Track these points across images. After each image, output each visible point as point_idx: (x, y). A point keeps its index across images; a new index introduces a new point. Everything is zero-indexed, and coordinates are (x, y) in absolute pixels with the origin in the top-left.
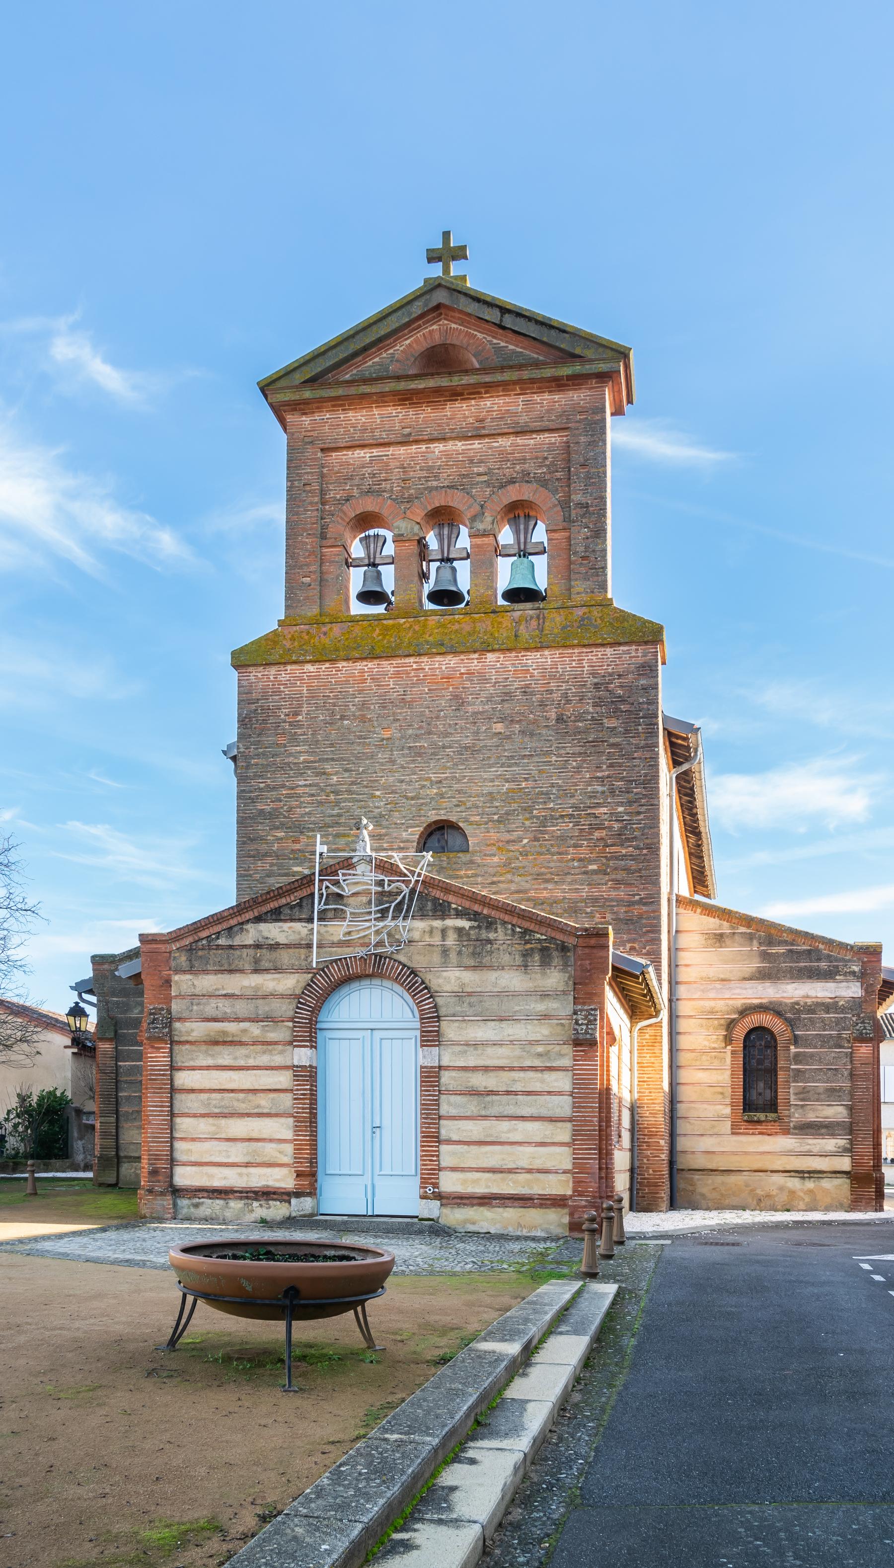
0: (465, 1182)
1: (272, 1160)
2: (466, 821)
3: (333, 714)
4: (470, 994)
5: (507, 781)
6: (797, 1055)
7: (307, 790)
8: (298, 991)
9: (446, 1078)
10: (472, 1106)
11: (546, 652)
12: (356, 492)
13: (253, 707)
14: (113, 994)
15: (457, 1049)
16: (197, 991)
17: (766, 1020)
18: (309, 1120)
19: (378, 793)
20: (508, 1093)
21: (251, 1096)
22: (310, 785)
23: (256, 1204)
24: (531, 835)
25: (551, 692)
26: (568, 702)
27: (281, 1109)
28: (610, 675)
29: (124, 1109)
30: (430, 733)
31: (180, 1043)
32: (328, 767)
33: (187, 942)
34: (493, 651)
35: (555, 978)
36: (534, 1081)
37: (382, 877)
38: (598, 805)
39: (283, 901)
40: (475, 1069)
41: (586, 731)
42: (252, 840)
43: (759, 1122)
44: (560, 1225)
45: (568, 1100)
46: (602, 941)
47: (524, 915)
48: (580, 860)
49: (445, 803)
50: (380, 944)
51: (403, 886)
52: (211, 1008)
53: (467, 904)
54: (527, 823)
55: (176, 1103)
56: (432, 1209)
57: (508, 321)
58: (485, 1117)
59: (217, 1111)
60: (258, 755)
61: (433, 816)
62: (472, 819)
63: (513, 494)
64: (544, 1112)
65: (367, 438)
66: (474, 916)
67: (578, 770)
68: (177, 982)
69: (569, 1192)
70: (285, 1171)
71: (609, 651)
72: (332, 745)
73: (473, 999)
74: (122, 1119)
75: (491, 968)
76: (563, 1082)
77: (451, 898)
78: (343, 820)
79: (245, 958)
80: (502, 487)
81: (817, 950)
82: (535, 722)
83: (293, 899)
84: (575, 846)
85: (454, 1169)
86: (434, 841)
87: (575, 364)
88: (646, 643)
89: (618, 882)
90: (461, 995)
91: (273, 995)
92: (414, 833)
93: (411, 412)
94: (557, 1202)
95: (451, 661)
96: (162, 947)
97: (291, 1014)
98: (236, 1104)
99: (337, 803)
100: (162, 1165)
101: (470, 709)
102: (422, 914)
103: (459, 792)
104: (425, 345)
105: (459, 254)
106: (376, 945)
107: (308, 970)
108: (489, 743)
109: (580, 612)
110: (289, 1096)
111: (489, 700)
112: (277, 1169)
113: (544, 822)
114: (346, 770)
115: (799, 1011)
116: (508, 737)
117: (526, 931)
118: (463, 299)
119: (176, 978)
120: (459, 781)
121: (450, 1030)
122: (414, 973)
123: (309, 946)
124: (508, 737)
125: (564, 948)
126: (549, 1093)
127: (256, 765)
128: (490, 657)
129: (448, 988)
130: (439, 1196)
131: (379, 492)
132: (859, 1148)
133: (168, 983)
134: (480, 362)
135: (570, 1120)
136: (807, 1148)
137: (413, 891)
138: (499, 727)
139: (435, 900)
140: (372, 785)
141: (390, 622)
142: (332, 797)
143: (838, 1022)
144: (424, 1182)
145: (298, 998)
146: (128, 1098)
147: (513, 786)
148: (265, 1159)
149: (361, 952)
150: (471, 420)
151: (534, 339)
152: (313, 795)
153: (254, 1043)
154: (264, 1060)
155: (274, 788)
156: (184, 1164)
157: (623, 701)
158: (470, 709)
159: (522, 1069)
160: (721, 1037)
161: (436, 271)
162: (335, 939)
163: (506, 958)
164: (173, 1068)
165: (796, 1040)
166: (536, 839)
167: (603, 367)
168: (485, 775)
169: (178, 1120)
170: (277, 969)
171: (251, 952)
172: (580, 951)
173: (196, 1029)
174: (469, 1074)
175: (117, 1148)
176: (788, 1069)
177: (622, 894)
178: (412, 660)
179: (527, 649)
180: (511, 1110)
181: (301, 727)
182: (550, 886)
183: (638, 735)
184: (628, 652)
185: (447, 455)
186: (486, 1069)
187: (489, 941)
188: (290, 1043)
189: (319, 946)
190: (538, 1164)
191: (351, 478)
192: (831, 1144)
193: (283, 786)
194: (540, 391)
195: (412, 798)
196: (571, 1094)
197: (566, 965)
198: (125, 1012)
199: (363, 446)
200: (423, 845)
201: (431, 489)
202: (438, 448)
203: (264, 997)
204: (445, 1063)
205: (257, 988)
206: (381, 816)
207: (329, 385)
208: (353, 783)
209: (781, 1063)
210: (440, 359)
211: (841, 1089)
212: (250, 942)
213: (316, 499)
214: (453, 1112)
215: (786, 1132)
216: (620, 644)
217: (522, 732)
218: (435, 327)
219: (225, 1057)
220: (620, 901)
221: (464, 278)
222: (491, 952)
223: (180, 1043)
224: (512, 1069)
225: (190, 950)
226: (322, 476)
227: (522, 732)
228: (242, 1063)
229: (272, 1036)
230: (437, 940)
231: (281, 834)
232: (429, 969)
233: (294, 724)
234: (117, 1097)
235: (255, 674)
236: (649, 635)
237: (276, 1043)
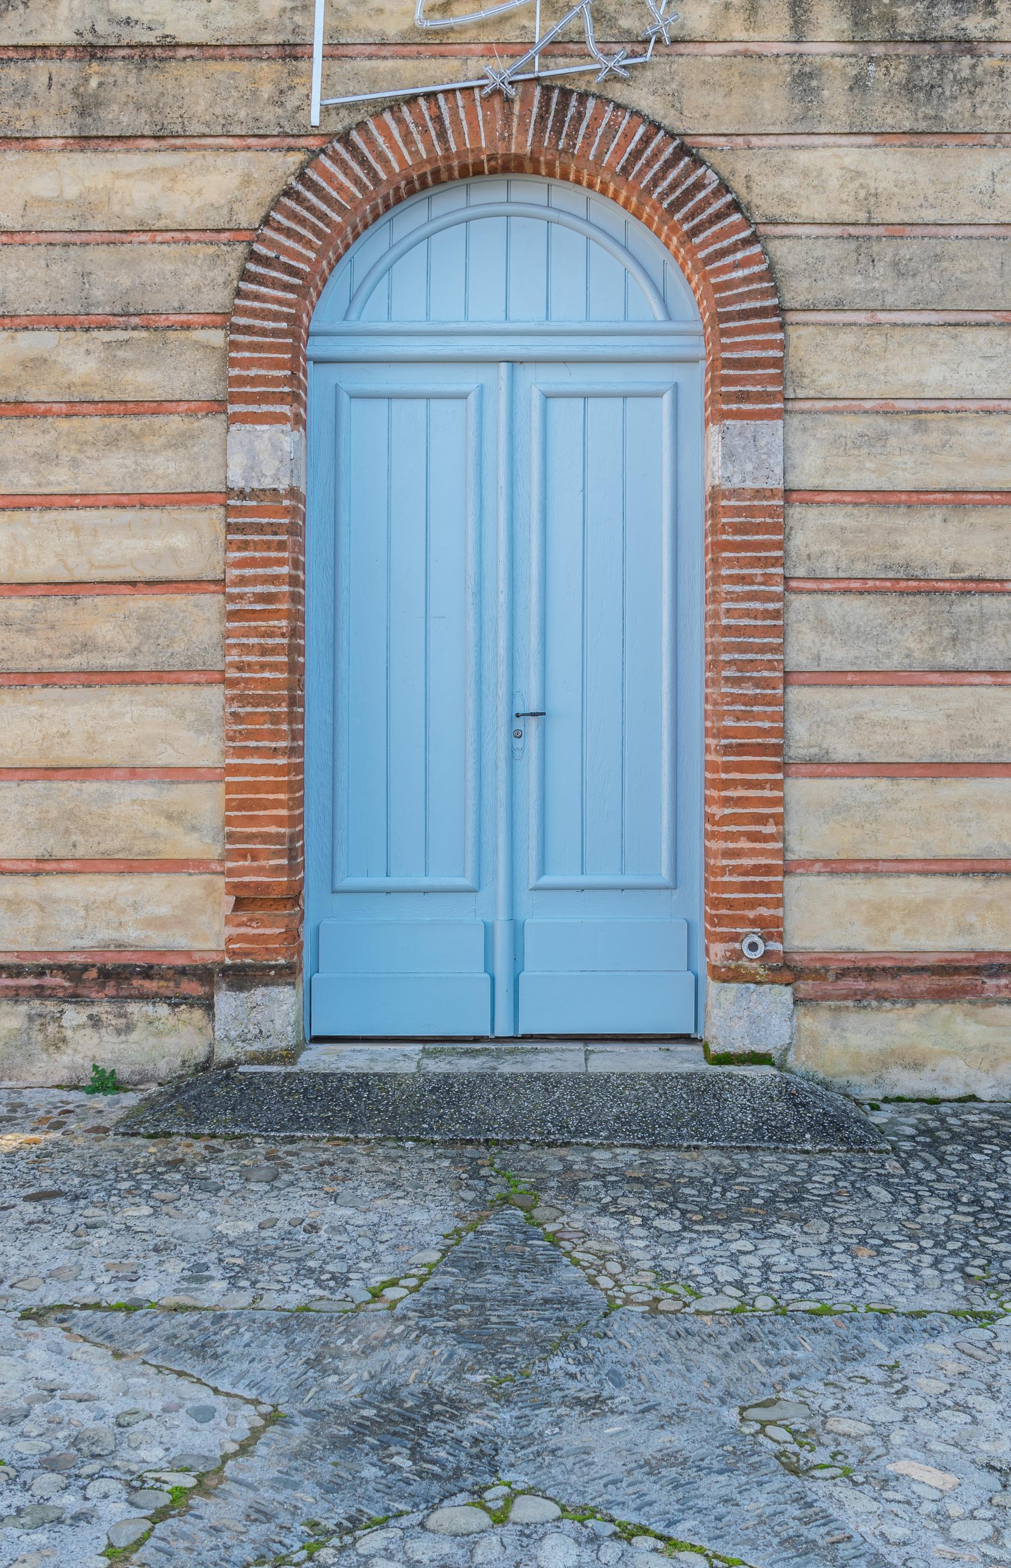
1: (139, 848)
4: (897, 231)
8: (248, 216)
9: (810, 533)
10: (907, 635)
15: (854, 425)
21: (57, 608)
23: (74, 1016)
40: (916, 499)
56: (750, 1018)
58: (956, 675)
70: (188, 887)
73: (908, 250)
75: (970, 137)
85: (838, 867)
90: (865, 233)
97: (219, 298)
110: (212, 603)
112: (157, 883)
121: (824, 359)
129: (815, 208)
130: (785, 970)
148: (112, 844)
149: (498, 70)
154: (112, 470)
171: (67, 71)
174: (898, 519)
186: (958, 499)
187: (965, 44)
188: (216, 406)
203: (117, 237)
204: (805, 477)
205: (86, 206)
214: (838, 655)
229: (143, 381)
237: (158, 407)
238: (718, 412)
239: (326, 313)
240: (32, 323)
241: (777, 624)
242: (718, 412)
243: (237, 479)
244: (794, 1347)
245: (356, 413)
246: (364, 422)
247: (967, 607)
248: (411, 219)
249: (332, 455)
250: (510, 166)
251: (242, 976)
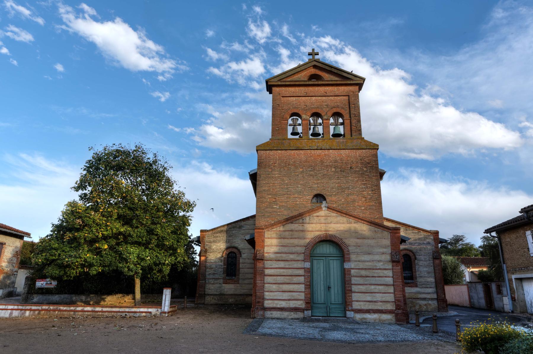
3: (286, 163)
17: (408, 252)
20: (373, 277)
38: (364, 191)
41: (359, 171)
46: (398, 231)
58: (366, 284)
64: (385, 283)
65: (294, 95)
67: (357, 181)
69: (394, 309)
70: (302, 302)
85: (357, 301)
99: (287, 188)
104: (310, 74)
110: (303, 277)
135: (304, 284)
147: (339, 185)
156: (268, 300)
160: (353, 257)
196: (393, 277)
201: (312, 108)
210: (313, 77)
231: (270, 196)
233: (274, 166)
237: (298, 261)
244: (318, 187)
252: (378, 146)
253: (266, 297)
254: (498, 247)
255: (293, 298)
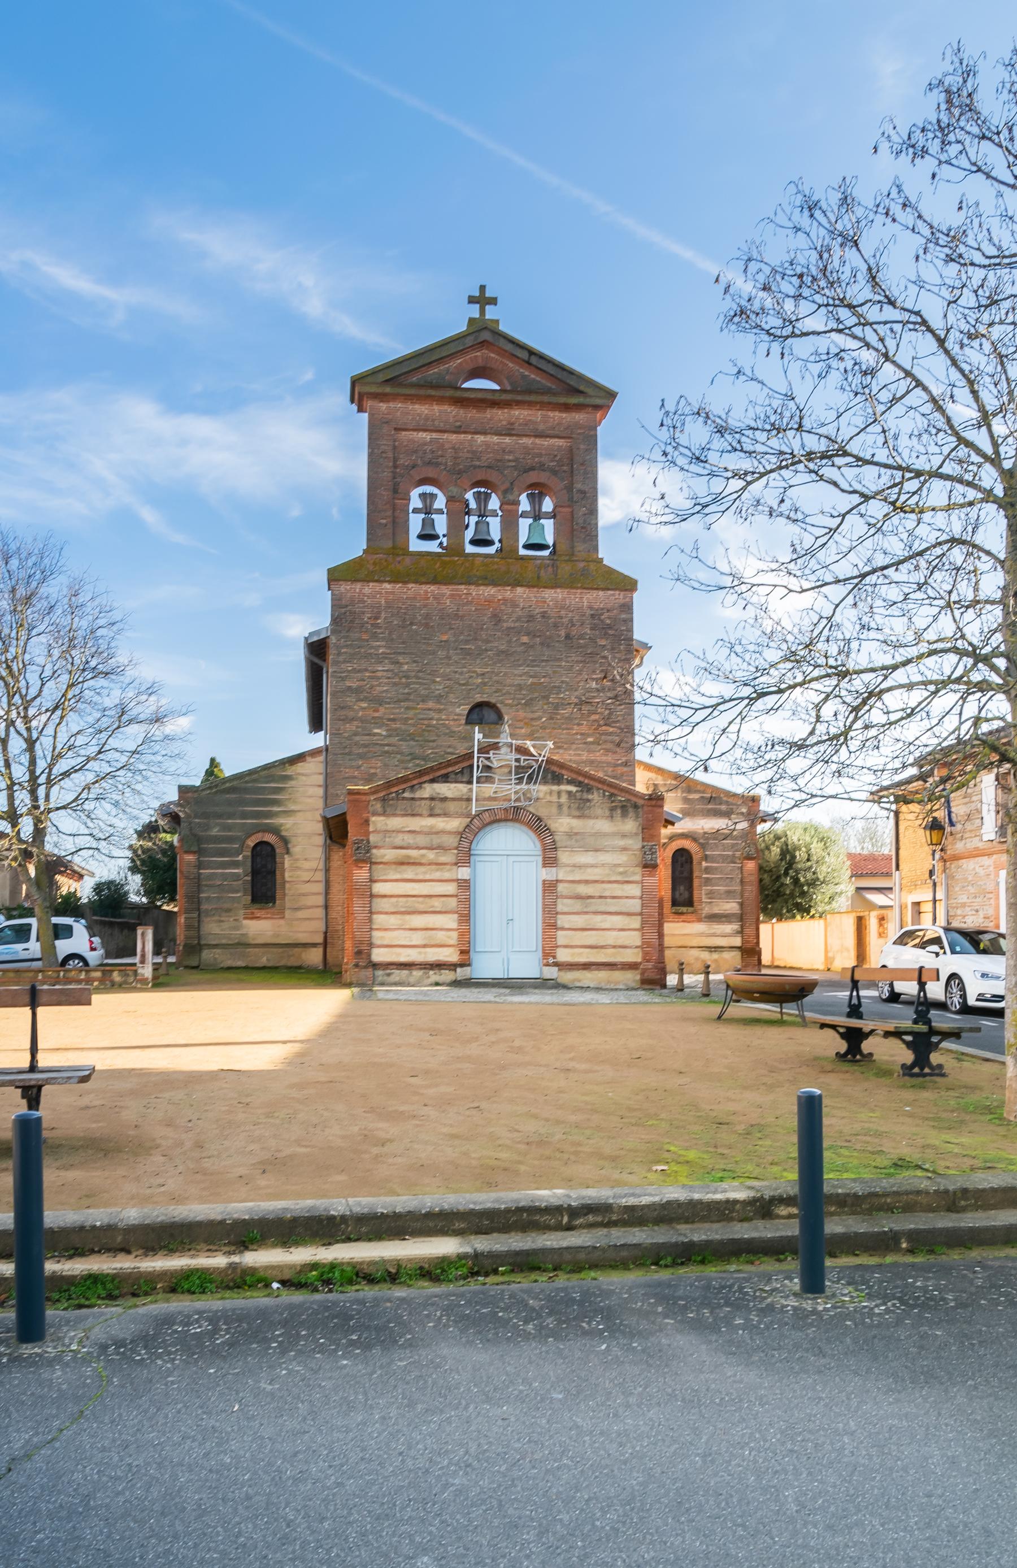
0: (573, 955)
1: (443, 943)
2: (502, 703)
3: (404, 620)
4: (576, 834)
5: (531, 677)
6: (707, 868)
7: (385, 674)
8: (461, 830)
9: (561, 887)
10: (577, 906)
11: (558, 590)
12: (419, 462)
13: (343, 610)
14: (196, 817)
15: (569, 869)
16: (389, 828)
17: (687, 844)
18: (466, 917)
19: (438, 679)
20: (601, 897)
21: (427, 900)
22: (387, 671)
23: (431, 972)
24: (548, 716)
25: (561, 618)
26: (573, 625)
27: (449, 908)
28: (602, 609)
29: (204, 906)
30: (476, 639)
31: (376, 863)
32: (401, 659)
33: (382, 794)
34: (522, 586)
35: (630, 825)
36: (617, 890)
37: (518, 756)
39: (450, 769)
40: (579, 882)
41: (585, 646)
42: (343, 708)
43: (682, 913)
44: (634, 981)
45: (639, 901)
46: (659, 803)
47: (611, 785)
48: (582, 734)
49: (487, 689)
50: (518, 800)
51: (534, 763)
52: (399, 840)
53: (574, 776)
54: (545, 707)
55: (374, 905)
56: (551, 973)
57: (534, 360)
58: (586, 913)
59: (403, 910)
60: (347, 646)
61: (478, 698)
62: (507, 702)
63: (533, 477)
64: (624, 910)
66: (579, 784)
68: (374, 822)
70: (451, 950)
71: (601, 593)
72: (403, 643)
73: (578, 837)
74: (202, 915)
75: (589, 817)
76: (635, 890)
77: (564, 772)
78: (412, 697)
79: (424, 807)
80: (525, 472)
81: (719, 798)
82: (550, 637)
83: (457, 768)
84: (578, 725)
85: (566, 947)
86: (475, 716)
87: (578, 396)
88: (626, 590)
89: (607, 750)
90: (571, 834)
91: (443, 832)
92: (464, 710)
93: (462, 411)
94: (632, 966)
95: (489, 591)
96: (364, 798)
97: (456, 844)
98: (417, 905)
99: (407, 685)
100: (364, 947)
101: (505, 625)
102: (545, 781)
103: (498, 682)
105: (493, 301)
106: (515, 801)
107: (468, 815)
108: (519, 649)
109: (582, 565)
110: (455, 900)
111: (518, 619)
112: (445, 949)
113: (557, 707)
114: (415, 662)
115: (708, 839)
116: (532, 647)
117: (612, 795)
118: (502, 340)
119: (373, 819)
120: (497, 675)
121: (564, 857)
122: (539, 819)
123: (469, 800)
124: (532, 647)
125: (636, 806)
126: (627, 897)
127: (346, 653)
128: (519, 590)
129: (562, 829)
130: (556, 964)
131: (437, 464)
132: (747, 931)
133: (367, 822)
134: (511, 384)
135: (457, 912)
136: (713, 931)
137: (540, 767)
138: (525, 639)
139: (554, 772)
140: (434, 673)
141: (447, 559)
142: (404, 680)
143: (733, 845)
144: (546, 955)
145: (461, 834)
146: (208, 898)
147: (535, 680)
148: (438, 942)
149: (506, 805)
150: (504, 423)
151: (552, 375)
152: (389, 678)
153: (430, 864)
154: (437, 875)
155: (359, 671)
157: (610, 628)
158: (505, 625)
159: (610, 882)
161: (474, 311)
162: (487, 796)
163: (599, 812)
164: (372, 881)
165: (706, 858)
166: (551, 718)
167: (598, 401)
168: (516, 672)
169: (375, 916)
170: (446, 815)
171: (428, 802)
172: (646, 809)
173: (389, 854)
174: (575, 885)
175: (199, 938)
176: (700, 877)
177: (609, 758)
178: (463, 587)
179: (545, 587)
180: (602, 908)
181: (380, 628)
182: (561, 751)
183: (620, 652)
184: (613, 595)
185: (487, 444)
186: (587, 882)
187: (588, 800)
188: (456, 864)
189: (477, 800)
190: (620, 943)
191: (416, 452)
192: (730, 928)
193: (366, 670)
194: (553, 410)
195: (463, 685)
196: (641, 898)
197: (637, 817)
198: (206, 830)
199: (425, 430)
200: (469, 721)
201: (475, 467)
202: (480, 439)
203: (437, 833)
204: (560, 878)
205: (432, 827)
206: (441, 696)
207: (401, 385)
208: (419, 671)
209: (696, 874)
211: (734, 891)
212: (427, 796)
213: (391, 464)
214: (566, 910)
215: (700, 920)
216: (609, 589)
217: (542, 644)
218: (478, 354)
219: (409, 873)
220: (608, 764)
221: (497, 321)
222: (590, 808)
223: (376, 863)
224: (603, 882)
225: (384, 800)
226: (395, 448)
227: (542, 644)
228: (421, 877)
229: (443, 859)
230: (554, 798)
232: (549, 817)
233: (376, 626)
234: (198, 898)
235: (344, 587)
236: (629, 585)
237: (445, 864)
238: (544, 865)
239: (473, 846)
240: (422, 848)
241: (555, 904)
242: (544, 865)
243: (460, 877)
245: (478, 864)
246: (479, 865)
247: (589, 901)
248: (488, 828)
249: (474, 873)
250: (506, 820)
251: (462, 965)
252: (636, 582)
253: (377, 941)
254: (112, 917)
255: (433, 943)
